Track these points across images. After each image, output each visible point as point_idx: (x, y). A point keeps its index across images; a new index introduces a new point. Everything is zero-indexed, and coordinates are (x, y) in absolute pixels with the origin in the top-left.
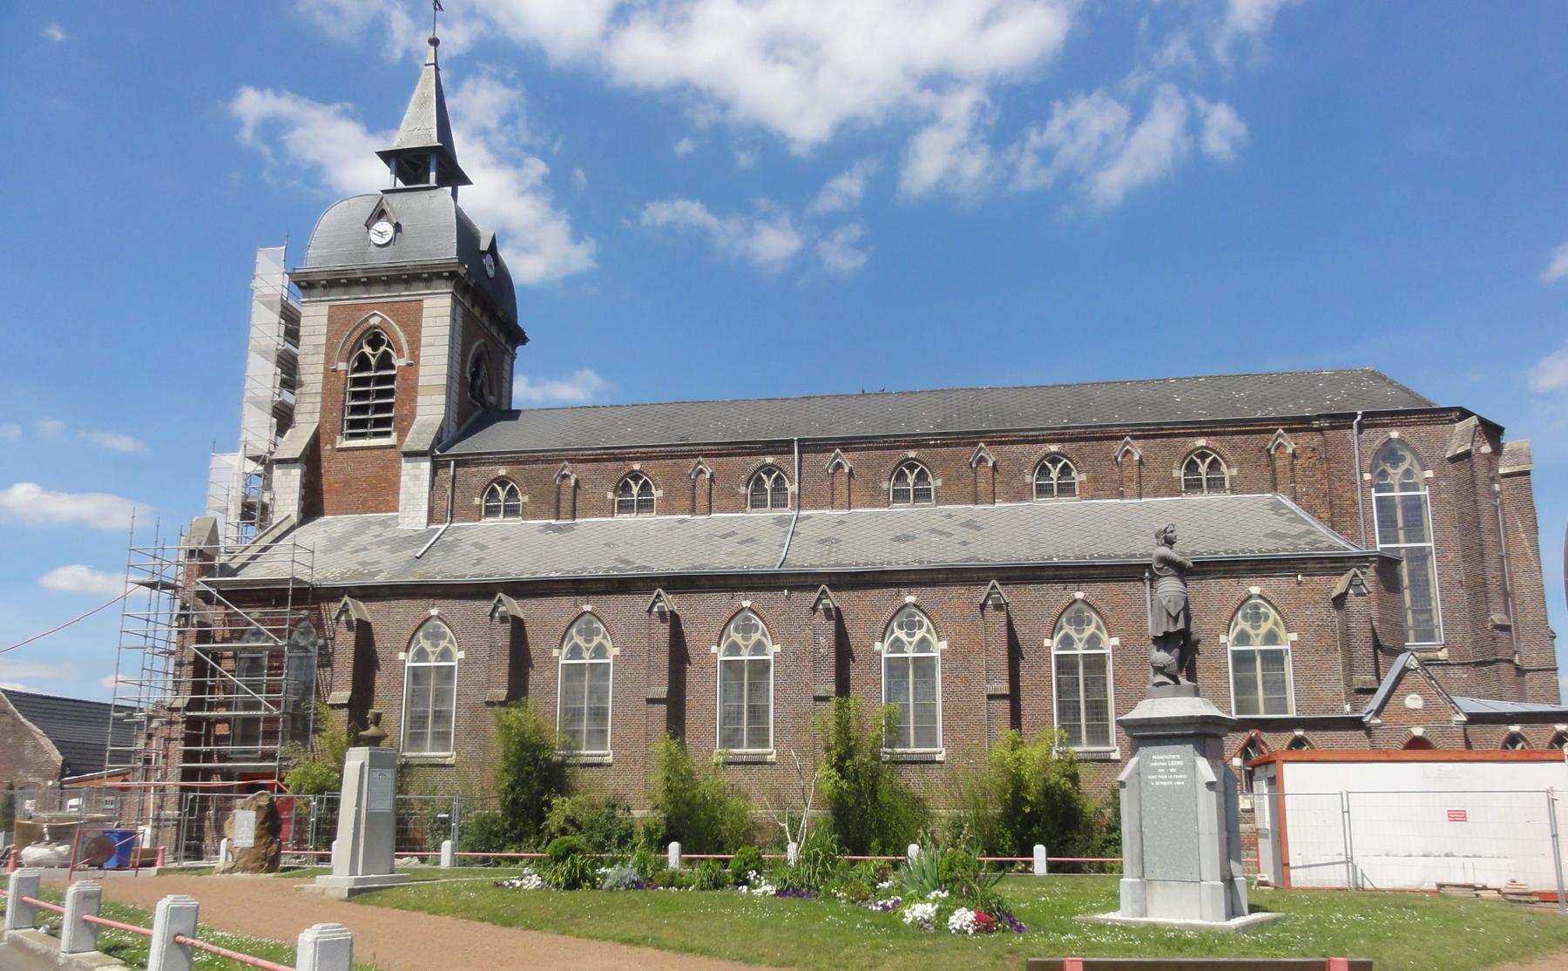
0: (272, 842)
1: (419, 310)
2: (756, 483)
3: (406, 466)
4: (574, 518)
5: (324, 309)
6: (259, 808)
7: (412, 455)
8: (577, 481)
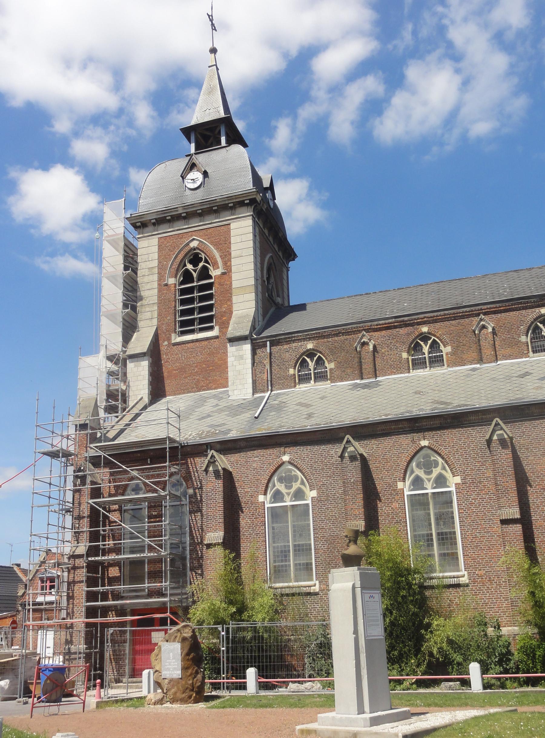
0: (197, 673)
1: (228, 233)
2: (534, 332)
3: (231, 349)
4: (376, 377)
5: (154, 241)
6: (184, 639)
7: (233, 340)
8: (375, 347)
